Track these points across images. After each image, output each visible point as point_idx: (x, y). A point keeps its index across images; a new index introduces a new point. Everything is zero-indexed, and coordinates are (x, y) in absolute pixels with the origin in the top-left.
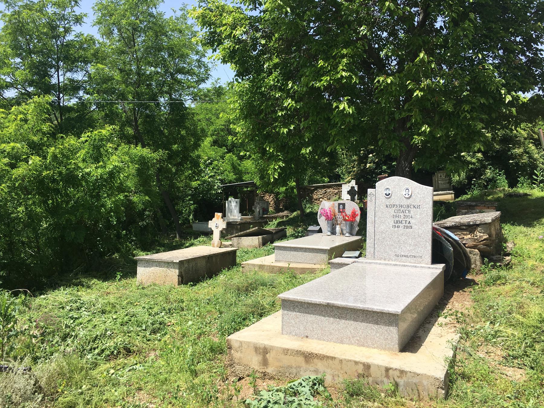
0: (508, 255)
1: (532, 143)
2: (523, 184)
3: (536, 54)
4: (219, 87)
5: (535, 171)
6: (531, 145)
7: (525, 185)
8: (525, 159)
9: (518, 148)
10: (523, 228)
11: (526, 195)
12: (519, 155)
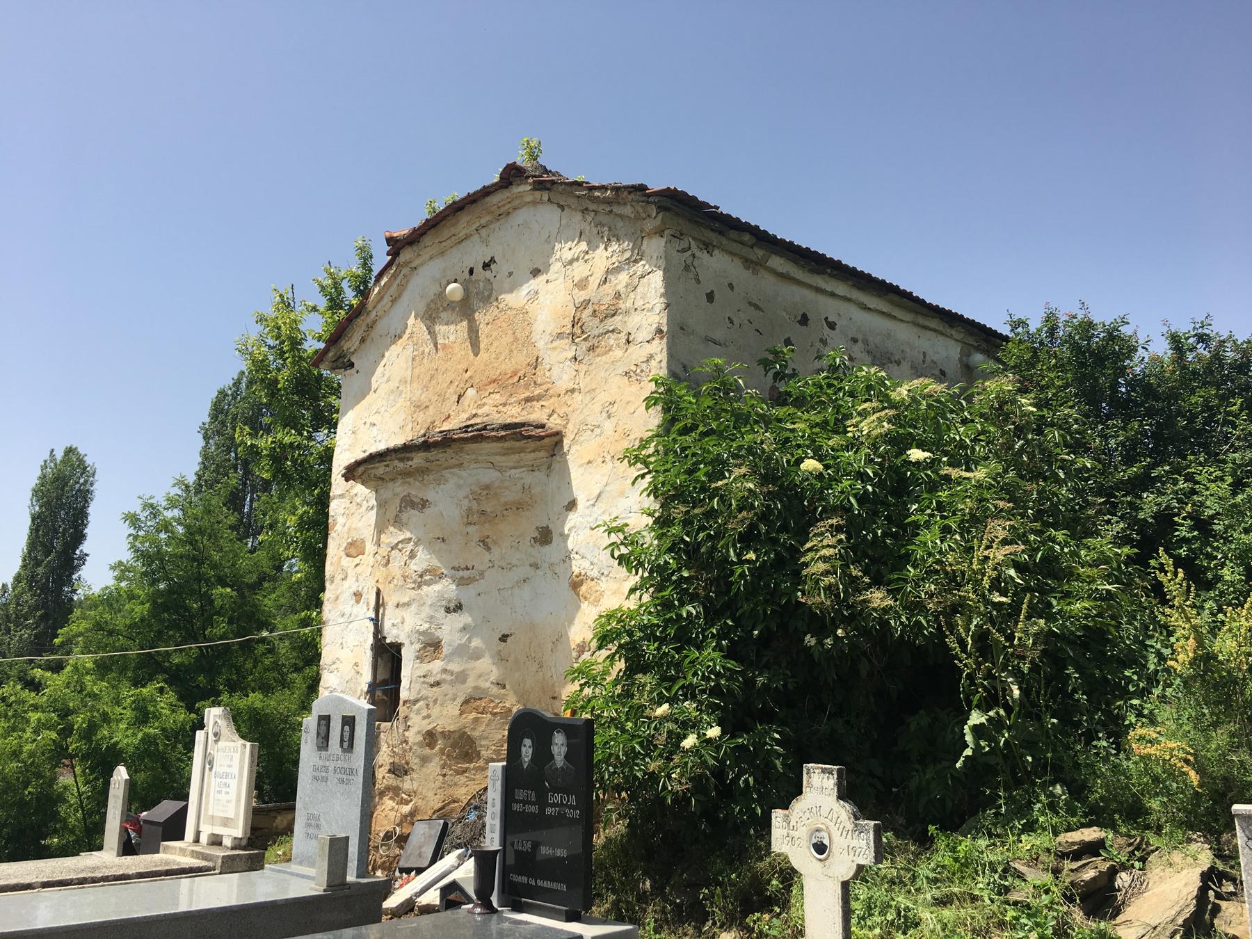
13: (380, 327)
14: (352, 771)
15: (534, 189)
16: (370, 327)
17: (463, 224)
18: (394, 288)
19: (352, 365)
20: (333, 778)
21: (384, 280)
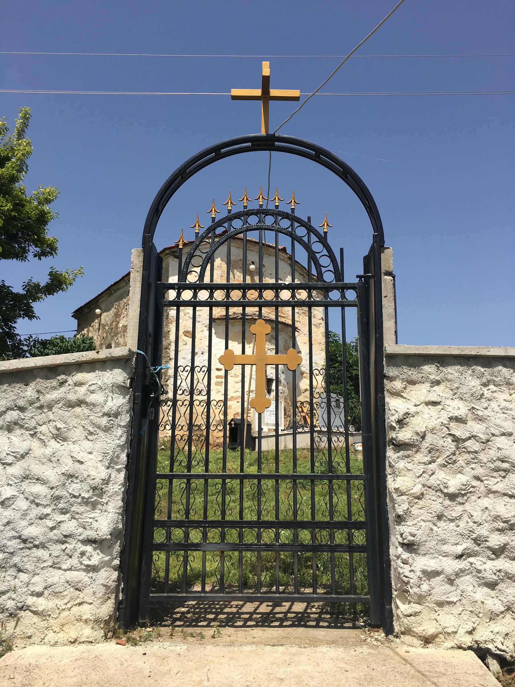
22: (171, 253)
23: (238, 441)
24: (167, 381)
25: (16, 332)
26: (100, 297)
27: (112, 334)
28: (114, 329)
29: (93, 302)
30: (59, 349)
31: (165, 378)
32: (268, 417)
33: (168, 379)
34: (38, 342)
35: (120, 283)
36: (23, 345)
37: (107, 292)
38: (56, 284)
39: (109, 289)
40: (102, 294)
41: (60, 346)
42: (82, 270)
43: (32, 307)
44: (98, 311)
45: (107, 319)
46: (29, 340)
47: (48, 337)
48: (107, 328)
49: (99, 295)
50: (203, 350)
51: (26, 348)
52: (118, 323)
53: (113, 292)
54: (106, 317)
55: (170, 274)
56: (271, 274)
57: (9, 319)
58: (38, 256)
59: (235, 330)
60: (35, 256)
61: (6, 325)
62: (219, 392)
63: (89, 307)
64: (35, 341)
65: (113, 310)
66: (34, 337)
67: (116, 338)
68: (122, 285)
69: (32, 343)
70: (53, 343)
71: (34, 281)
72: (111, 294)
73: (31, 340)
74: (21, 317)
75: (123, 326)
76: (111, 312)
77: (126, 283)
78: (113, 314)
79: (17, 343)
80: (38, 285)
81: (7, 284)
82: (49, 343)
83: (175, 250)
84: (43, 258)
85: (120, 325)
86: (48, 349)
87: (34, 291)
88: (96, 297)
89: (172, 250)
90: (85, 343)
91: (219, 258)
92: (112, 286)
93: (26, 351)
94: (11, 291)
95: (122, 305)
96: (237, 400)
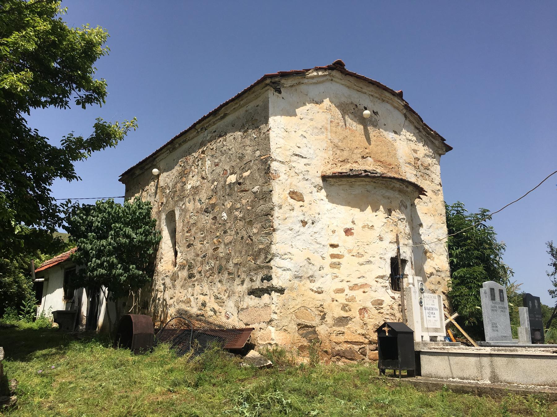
0: (14, 394)
1: (22, 272)
2: (9, 315)
3: (43, 192)
4: (379, 330)
5: (23, 302)
6: (21, 275)
7: (11, 315)
8: (14, 289)
9: (8, 276)
10: (23, 364)
11: (13, 326)
12: (9, 284)
13: (302, 87)
14: (505, 308)
15: (403, 106)
16: (299, 83)
17: (371, 89)
18: (322, 79)
19: (280, 92)
20: (499, 310)
21: (320, 73)
22: (271, 84)
23: (400, 359)
24: (269, 261)
25: (51, 195)
26: (158, 154)
27: (176, 199)
28: (178, 192)
29: (148, 161)
30: (106, 216)
31: (266, 258)
32: (428, 318)
33: (271, 259)
34: (78, 208)
35: (188, 133)
36: (60, 211)
37: (169, 146)
38: (103, 138)
39: (172, 142)
40: (161, 149)
41: (108, 212)
42: (135, 122)
43: (72, 165)
44: (155, 171)
45: (168, 180)
46: (67, 206)
47: (93, 203)
48: (168, 191)
49: (157, 151)
50: (313, 219)
51: (62, 215)
52: (185, 183)
53: (177, 146)
54: (167, 179)
55: (270, 112)
56: (385, 125)
57: (42, 180)
58: (83, 102)
59: (354, 193)
60: (78, 103)
61: (39, 187)
62: (337, 277)
63: (141, 169)
64: (74, 207)
65: (177, 168)
66: (73, 202)
67: (182, 203)
68: (191, 136)
69: (71, 210)
70: (99, 208)
71: (76, 135)
72: (174, 149)
73: (69, 205)
74: (58, 176)
75: (192, 187)
76: (174, 171)
77: (198, 132)
78: (176, 174)
79: (52, 209)
80: (80, 140)
81: (41, 134)
82: (94, 209)
83: (277, 79)
84: (87, 105)
85: (189, 187)
86: (92, 216)
87: (75, 148)
88: (154, 154)
89: (273, 80)
90: (142, 209)
91: (328, 99)
92: (177, 137)
93: (62, 219)
94: (46, 142)
95: (190, 162)
96: (362, 290)
